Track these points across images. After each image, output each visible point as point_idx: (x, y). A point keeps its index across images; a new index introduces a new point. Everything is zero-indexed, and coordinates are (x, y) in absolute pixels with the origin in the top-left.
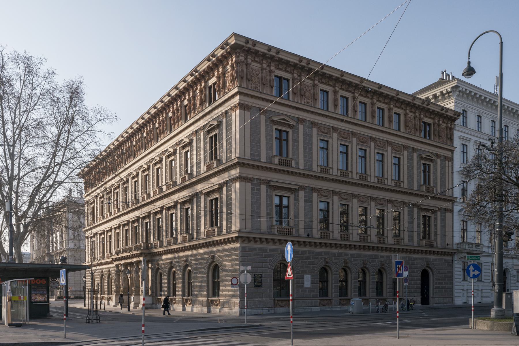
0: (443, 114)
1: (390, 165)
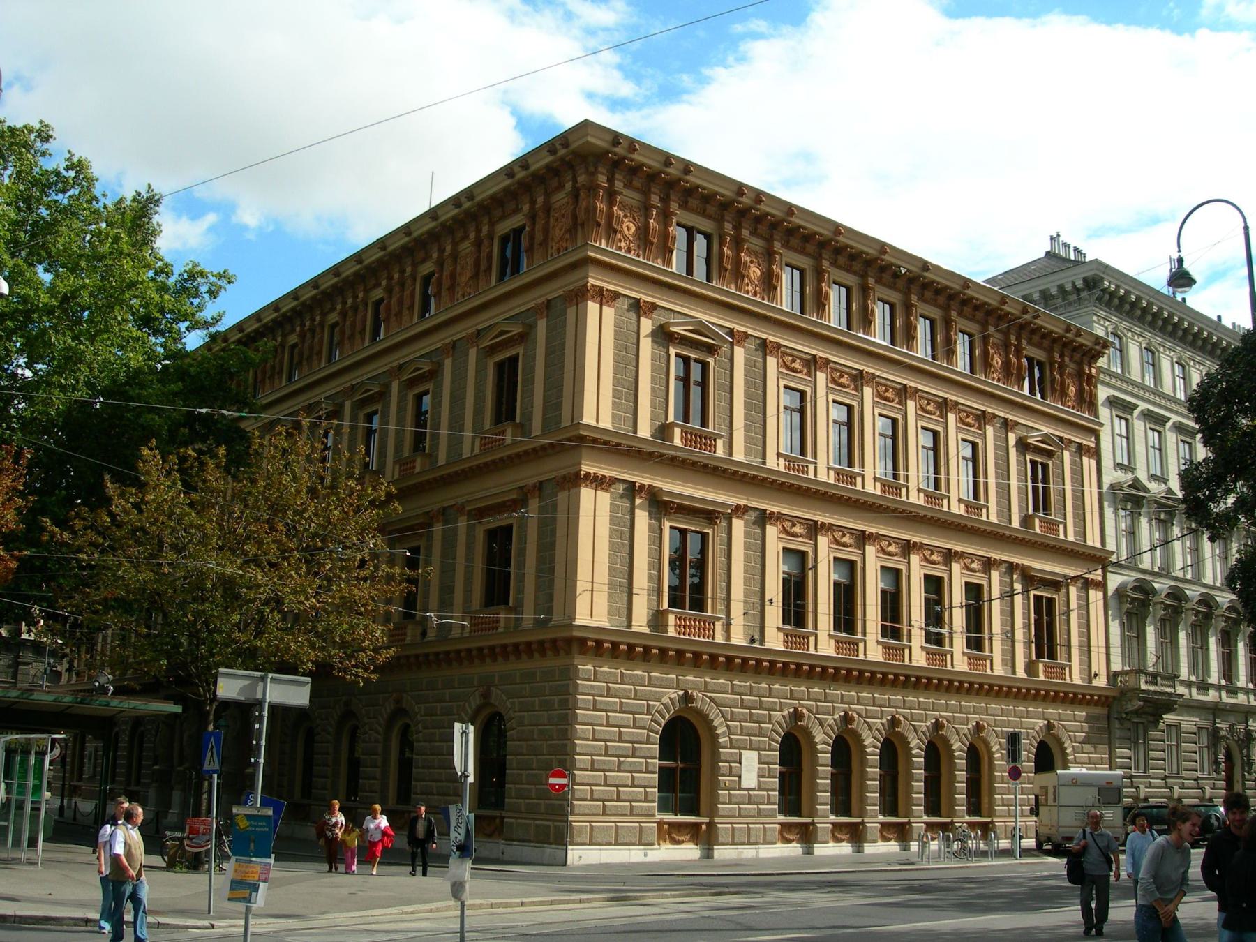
1: (953, 463)
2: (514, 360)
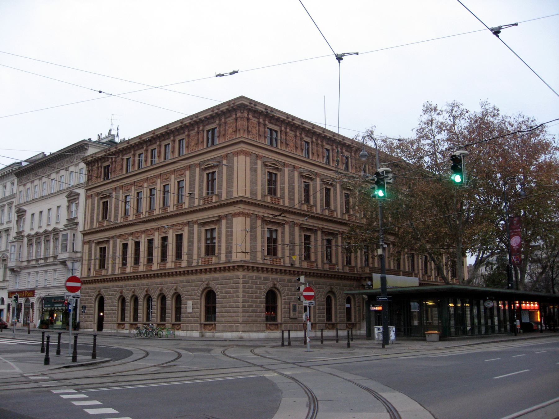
0: (289, 122)
2: (107, 202)
